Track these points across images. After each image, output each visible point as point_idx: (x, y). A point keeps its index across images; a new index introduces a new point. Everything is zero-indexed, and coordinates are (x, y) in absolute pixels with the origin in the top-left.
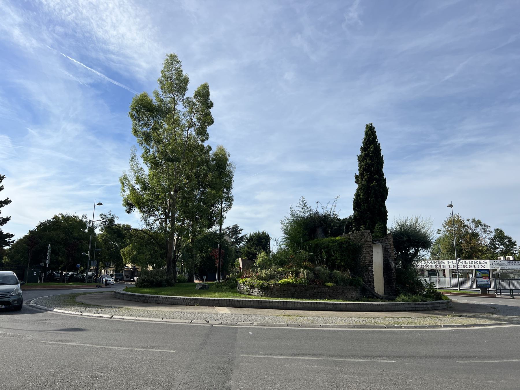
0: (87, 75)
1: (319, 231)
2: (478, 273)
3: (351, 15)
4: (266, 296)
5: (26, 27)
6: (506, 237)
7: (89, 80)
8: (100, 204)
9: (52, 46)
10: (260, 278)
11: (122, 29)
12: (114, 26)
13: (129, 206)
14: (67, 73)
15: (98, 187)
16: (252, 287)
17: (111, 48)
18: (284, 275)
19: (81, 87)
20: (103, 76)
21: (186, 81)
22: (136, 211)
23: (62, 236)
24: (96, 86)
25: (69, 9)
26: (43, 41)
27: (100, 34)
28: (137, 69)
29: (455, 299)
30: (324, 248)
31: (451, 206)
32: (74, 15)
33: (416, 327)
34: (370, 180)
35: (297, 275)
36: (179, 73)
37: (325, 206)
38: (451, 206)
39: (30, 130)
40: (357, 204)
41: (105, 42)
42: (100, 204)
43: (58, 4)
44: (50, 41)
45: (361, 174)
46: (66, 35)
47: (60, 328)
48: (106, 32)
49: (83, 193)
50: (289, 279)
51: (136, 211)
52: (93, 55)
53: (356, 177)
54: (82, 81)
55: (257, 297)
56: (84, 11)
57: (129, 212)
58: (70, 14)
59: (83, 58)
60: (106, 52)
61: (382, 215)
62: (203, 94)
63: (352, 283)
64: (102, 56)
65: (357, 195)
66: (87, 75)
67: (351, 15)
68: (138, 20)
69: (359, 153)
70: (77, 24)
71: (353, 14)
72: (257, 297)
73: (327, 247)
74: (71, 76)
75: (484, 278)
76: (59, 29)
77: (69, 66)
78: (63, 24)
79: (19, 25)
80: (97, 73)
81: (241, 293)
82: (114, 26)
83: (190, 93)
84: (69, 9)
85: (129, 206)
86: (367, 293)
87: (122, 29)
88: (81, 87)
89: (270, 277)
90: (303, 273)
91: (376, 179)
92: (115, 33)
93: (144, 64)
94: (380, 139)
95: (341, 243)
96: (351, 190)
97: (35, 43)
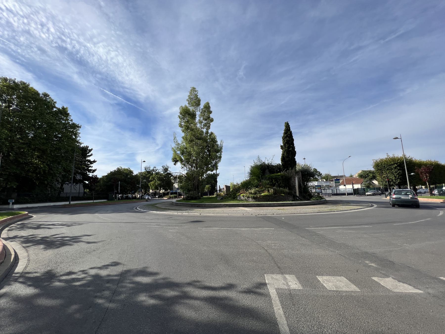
0: (114, 99)
1: (267, 171)
2: (316, 187)
3: (240, 73)
4: (256, 201)
5: (80, 74)
6: (318, 172)
7: (116, 102)
8: (144, 161)
9: (95, 84)
10: (251, 193)
11: (131, 77)
12: (127, 75)
13: (175, 161)
14: (104, 98)
15: (124, 154)
16: (248, 197)
17: (126, 86)
18: (263, 191)
19: (111, 105)
20: (122, 99)
21: (199, 101)
22: (179, 164)
23: (123, 177)
24: (119, 104)
25: (103, 66)
26: (90, 81)
27: (120, 79)
28: (140, 96)
29: (328, 199)
30: (274, 179)
31: (305, 159)
32: (106, 69)
33: (341, 211)
34: (289, 148)
35: (268, 191)
36: (196, 96)
37: (268, 159)
38: (305, 159)
39: (86, 126)
40: (283, 159)
41: (123, 83)
42: (144, 161)
43: (97, 63)
44: (94, 82)
45: (285, 145)
46: (102, 79)
47: (189, 221)
48: (123, 78)
49: (116, 157)
50: (266, 193)
51: (179, 164)
52: (117, 89)
53: (281, 146)
54: (112, 102)
55: (251, 202)
56: (111, 67)
57: (175, 164)
58: (104, 68)
59: (112, 91)
60: (124, 88)
61: (294, 163)
62: (207, 107)
63: (289, 194)
64: (121, 90)
65: (283, 155)
66: (114, 99)
67: (240, 73)
68: (139, 72)
69: (283, 135)
70: (108, 73)
71: (241, 73)
72: (251, 202)
73: (276, 178)
74: (106, 100)
75: (319, 189)
76: (98, 76)
77: (105, 95)
78: (100, 73)
79: (77, 73)
80: (120, 98)
81: (242, 200)
82: (127, 75)
83: (202, 106)
84: (103, 66)
85: (175, 161)
86: (295, 198)
87: (131, 77)
88: (111, 105)
89: (255, 193)
90: (272, 191)
91: (291, 147)
92: (128, 78)
93: (143, 94)
94: (292, 129)
95: (282, 176)
96: (280, 152)
97: (86, 82)
